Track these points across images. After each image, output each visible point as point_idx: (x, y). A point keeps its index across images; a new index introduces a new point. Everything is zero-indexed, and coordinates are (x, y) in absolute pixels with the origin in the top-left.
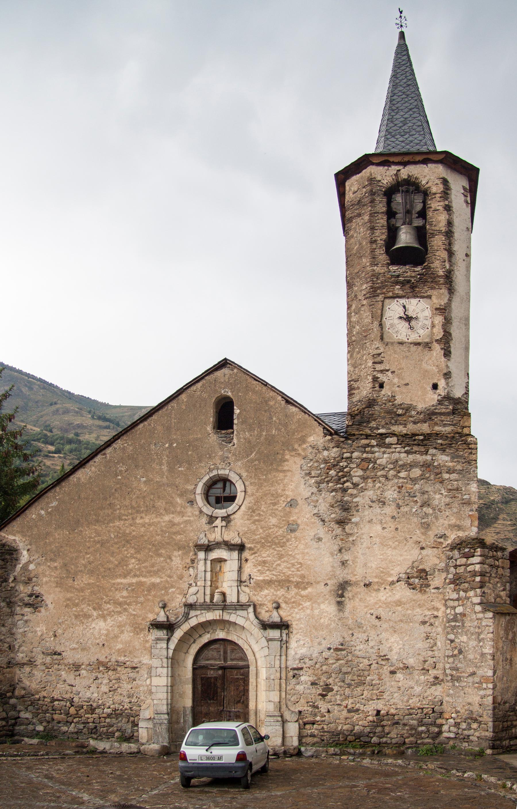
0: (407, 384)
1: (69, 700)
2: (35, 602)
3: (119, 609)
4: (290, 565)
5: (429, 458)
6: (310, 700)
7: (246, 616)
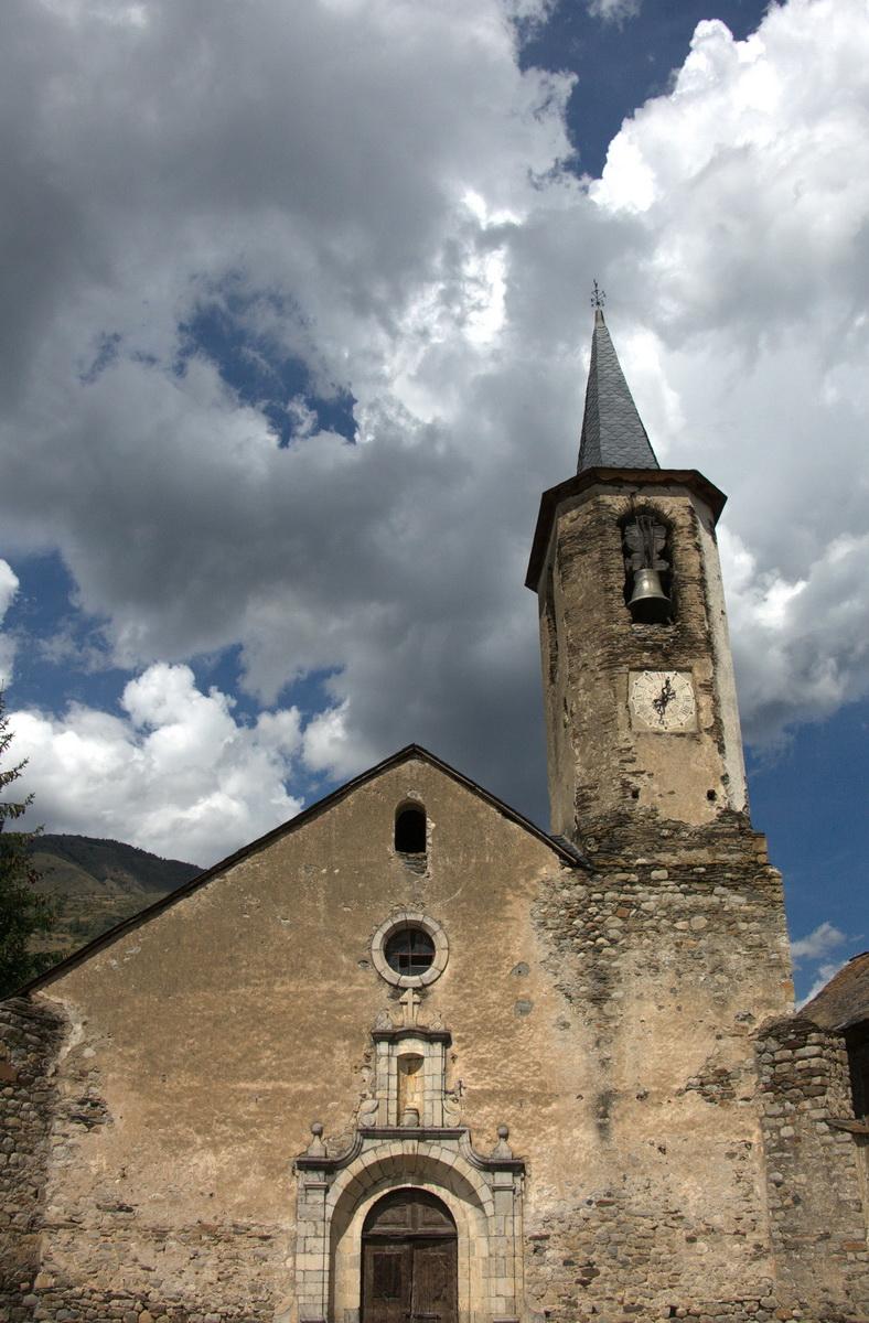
0: (672, 793)
3: (241, 1134)
5: (716, 899)
6: (564, 1292)
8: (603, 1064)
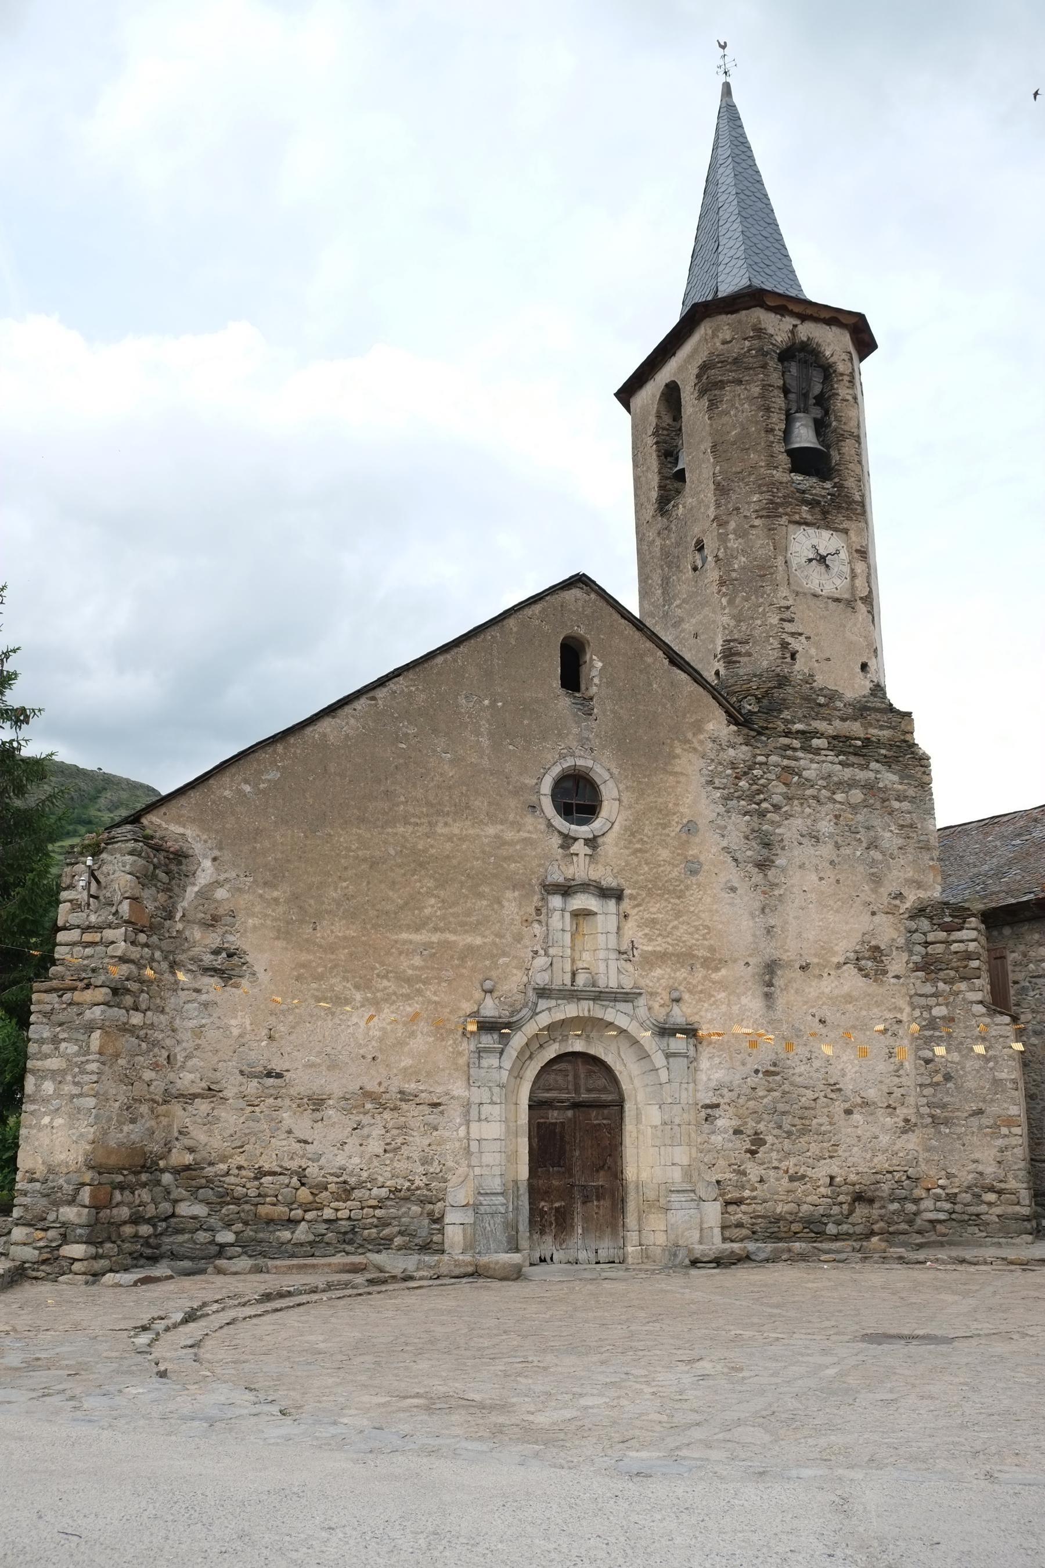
0: (828, 659)
1: (297, 1173)
2: (227, 967)
4: (692, 929)
6: (734, 1161)
7: (631, 1012)
8: (768, 932)
